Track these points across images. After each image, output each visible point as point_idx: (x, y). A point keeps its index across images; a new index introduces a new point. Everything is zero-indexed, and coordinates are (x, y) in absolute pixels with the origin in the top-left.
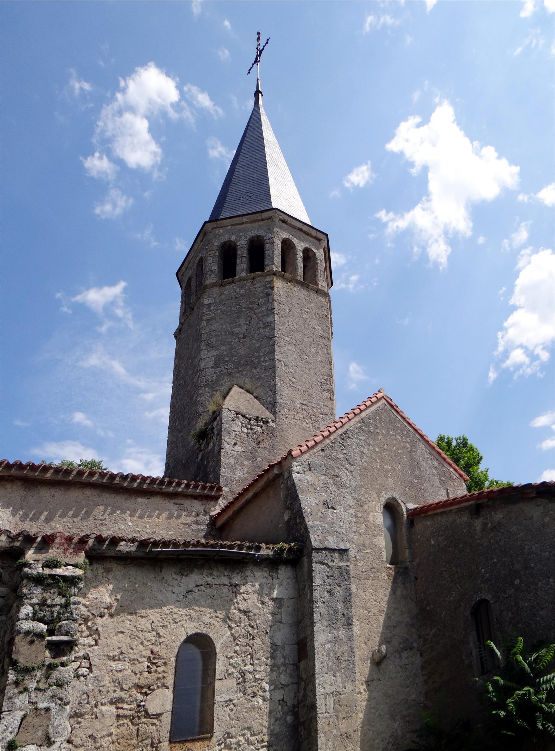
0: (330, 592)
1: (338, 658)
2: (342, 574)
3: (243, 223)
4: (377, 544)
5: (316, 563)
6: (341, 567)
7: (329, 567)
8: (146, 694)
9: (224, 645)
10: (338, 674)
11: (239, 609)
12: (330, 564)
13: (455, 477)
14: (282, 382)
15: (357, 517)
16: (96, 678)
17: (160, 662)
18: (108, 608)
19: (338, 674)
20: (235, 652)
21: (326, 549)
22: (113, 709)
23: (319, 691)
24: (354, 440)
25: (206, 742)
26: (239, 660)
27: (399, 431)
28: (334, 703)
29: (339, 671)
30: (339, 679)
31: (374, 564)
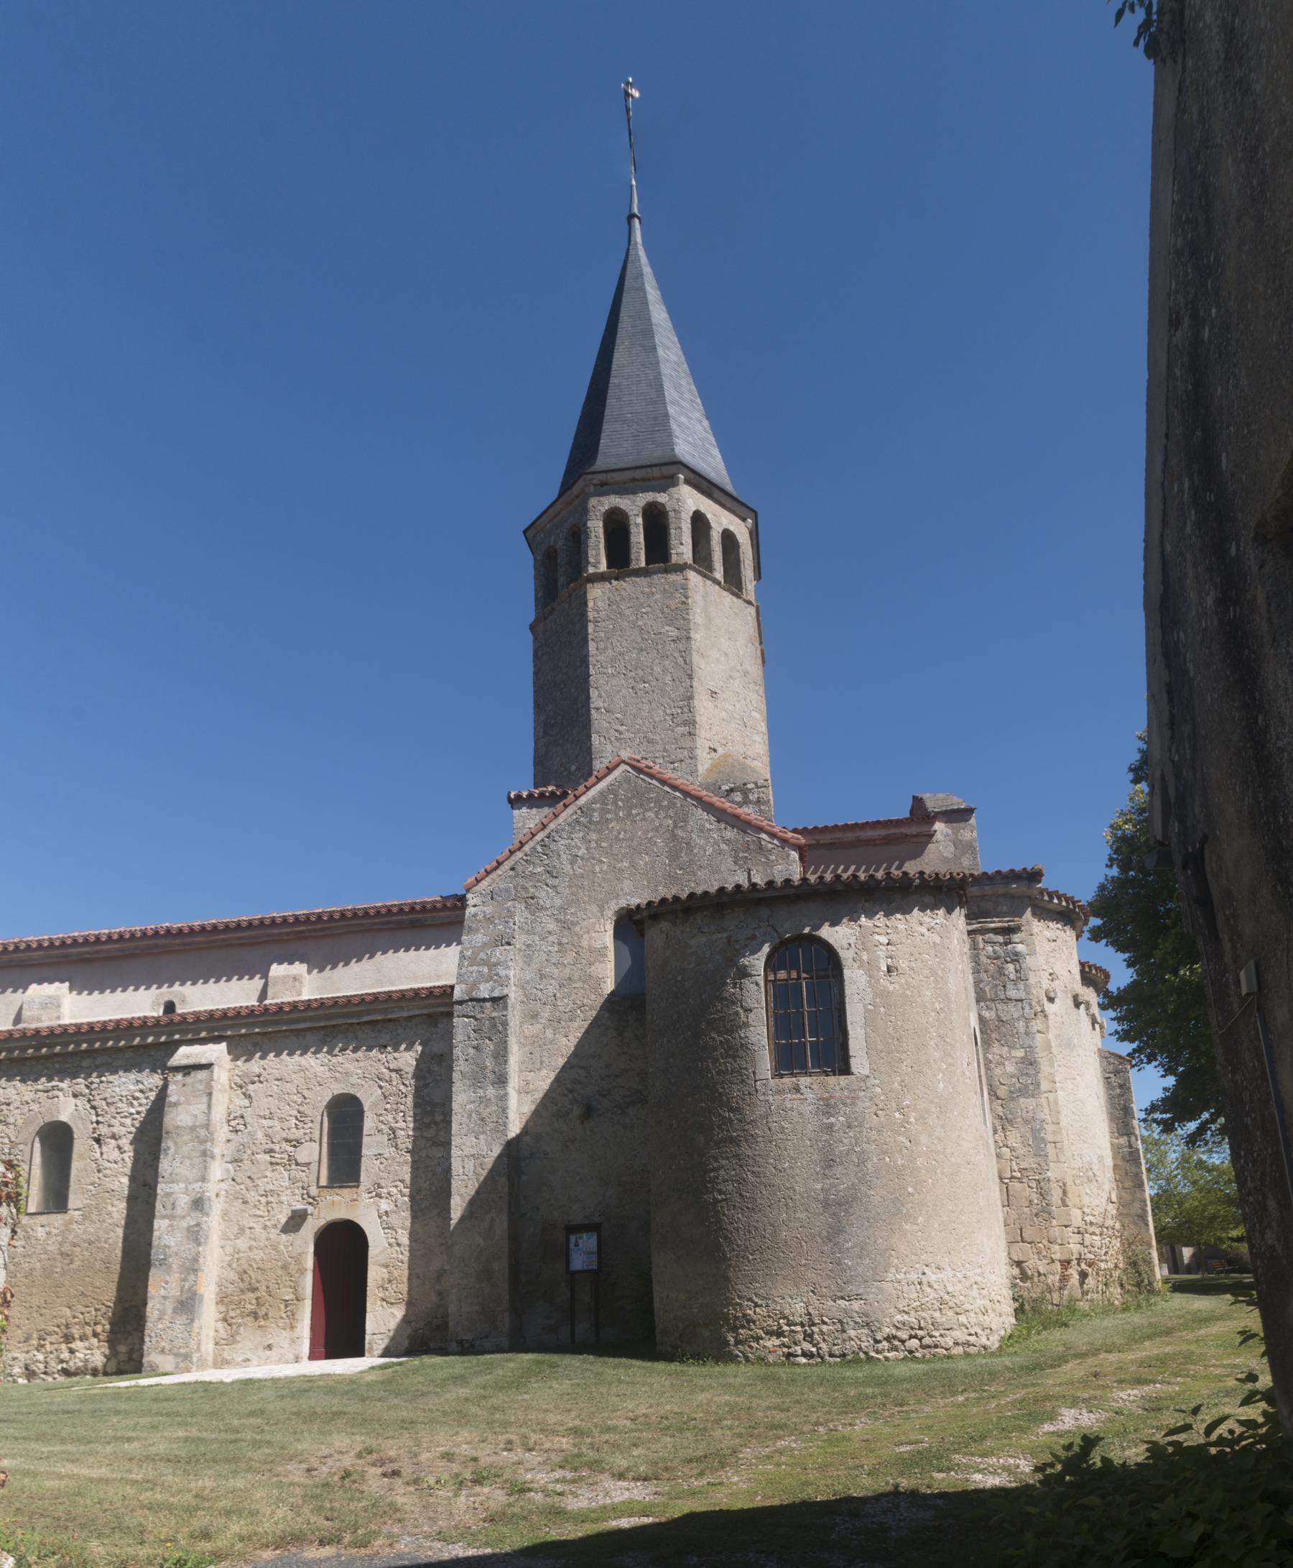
0: (476, 1048)
1: (483, 1119)
2: (494, 1026)
3: (559, 513)
4: (592, 974)
5: (458, 1017)
6: (494, 1018)
7: (476, 1019)
8: (295, 1146)
9: (375, 1104)
10: (481, 1137)
11: (388, 1069)
12: (478, 1016)
13: (770, 846)
14: (602, 739)
15: (560, 944)
16: (250, 1133)
17: (307, 1120)
18: (259, 1076)
19: (481, 1137)
20: (386, 1110)
21: (472, 1000)
22: (267, 1157)
23: (455, 1152)
24: (562, 842)
25: (355, 1189)
26: (390, 1118)
27: (652, 805)
28: (475, 1166)
29: (484, 1132)
30: (483, 1141)
31: (585, 1001)
